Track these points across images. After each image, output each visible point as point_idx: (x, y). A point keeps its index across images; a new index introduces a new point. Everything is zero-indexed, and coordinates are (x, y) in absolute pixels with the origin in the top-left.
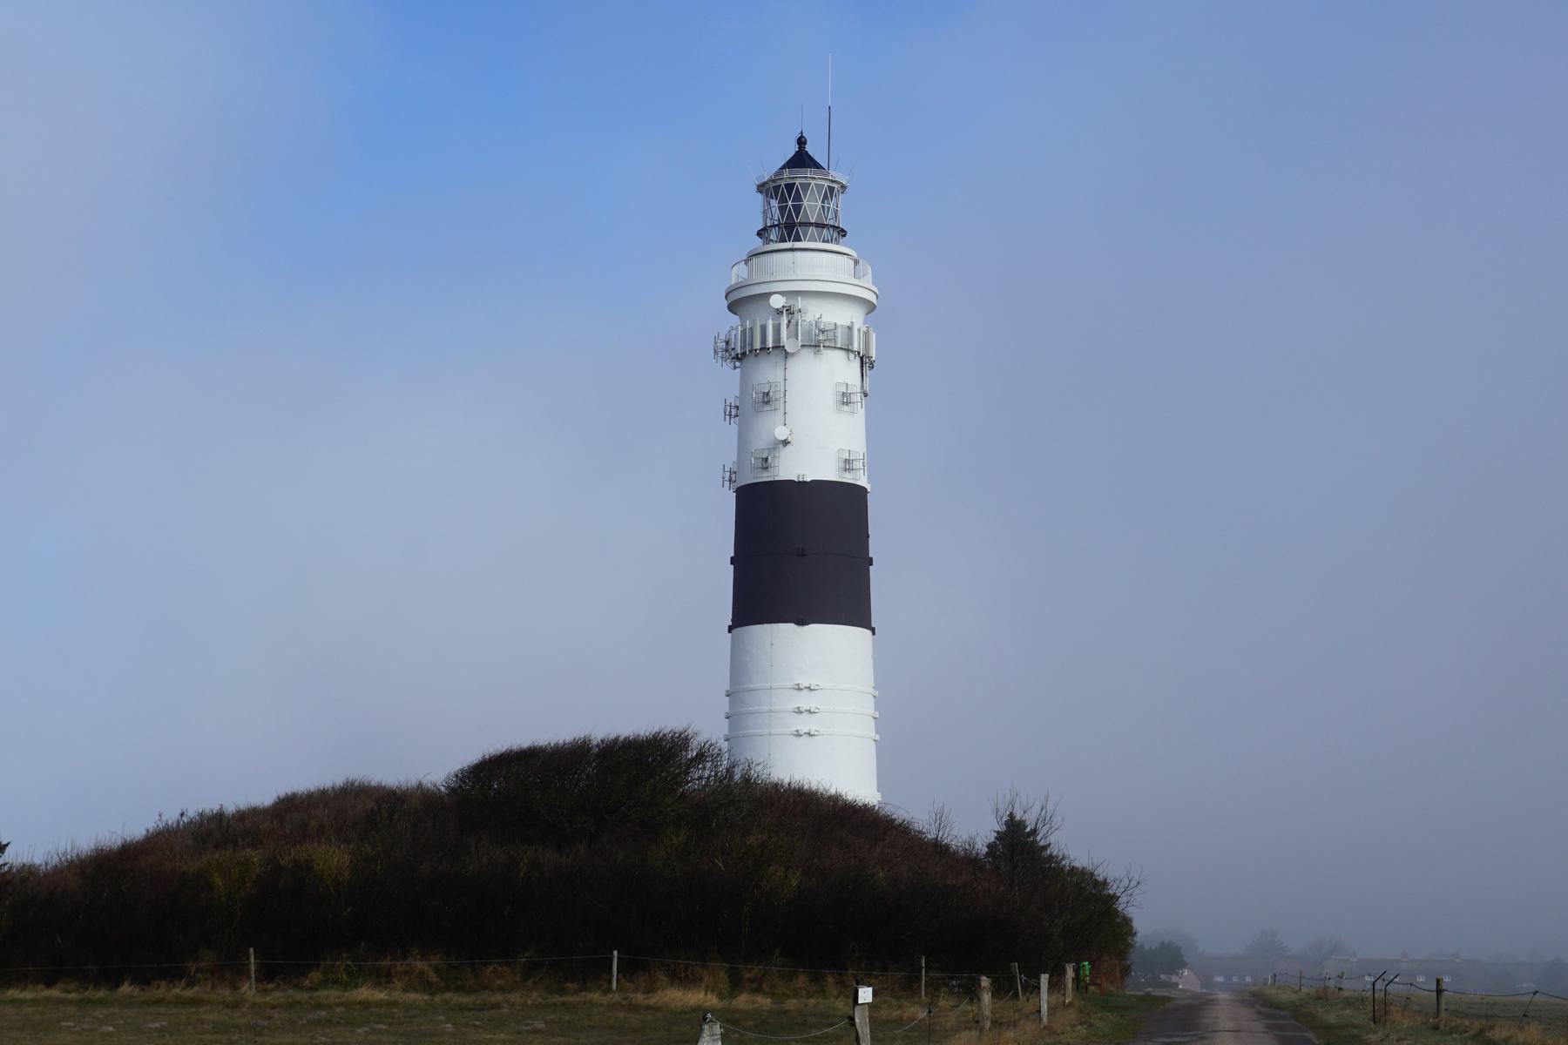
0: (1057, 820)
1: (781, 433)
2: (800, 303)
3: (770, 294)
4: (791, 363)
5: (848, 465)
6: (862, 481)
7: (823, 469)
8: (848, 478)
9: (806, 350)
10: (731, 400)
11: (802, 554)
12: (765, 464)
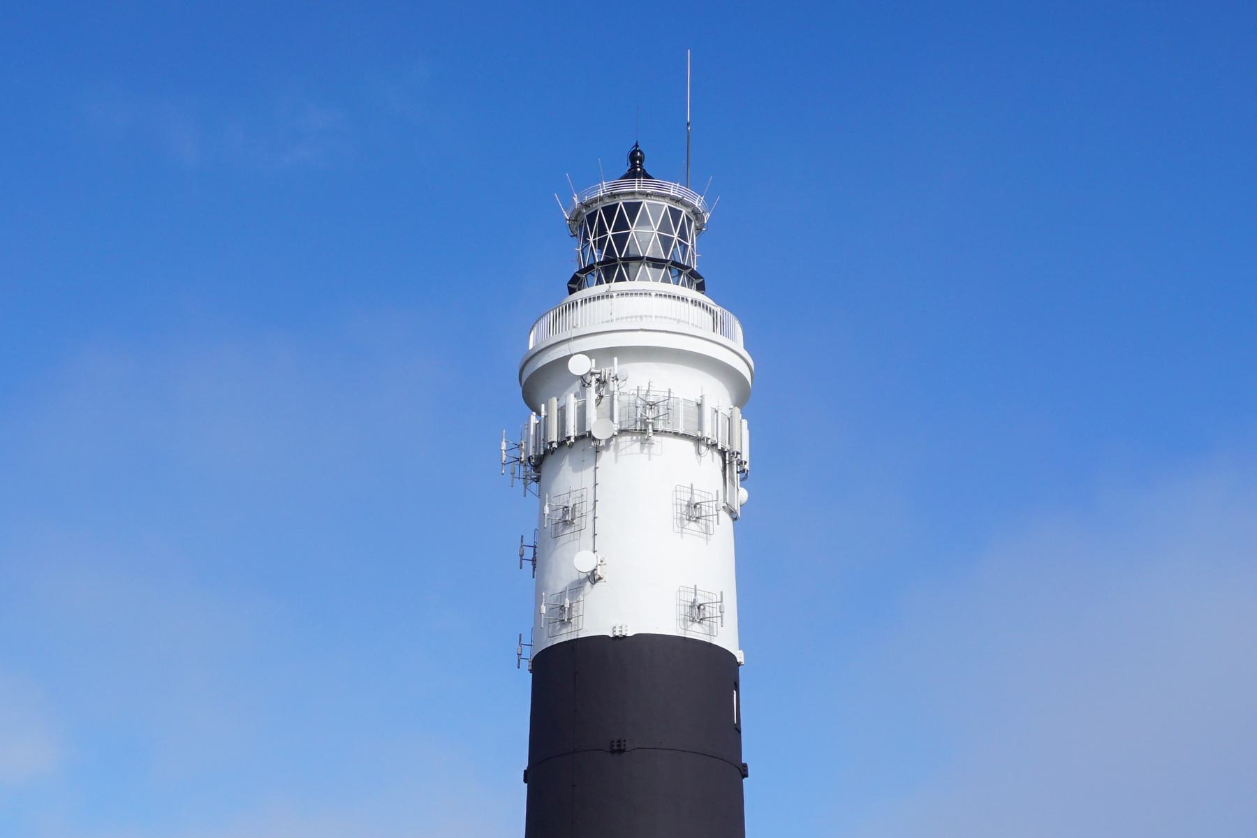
0: (520, 484)
1: (584, 561)
2: (616, 367)
3: (568, 357)
4: (606, 456)
5: (697, 611)
6: (726, 637)
7: (663, 620)
8: (696, 632)
9: (625, 439)
10: (745, 780)
11: (618, 749)
12: (562, 616)
